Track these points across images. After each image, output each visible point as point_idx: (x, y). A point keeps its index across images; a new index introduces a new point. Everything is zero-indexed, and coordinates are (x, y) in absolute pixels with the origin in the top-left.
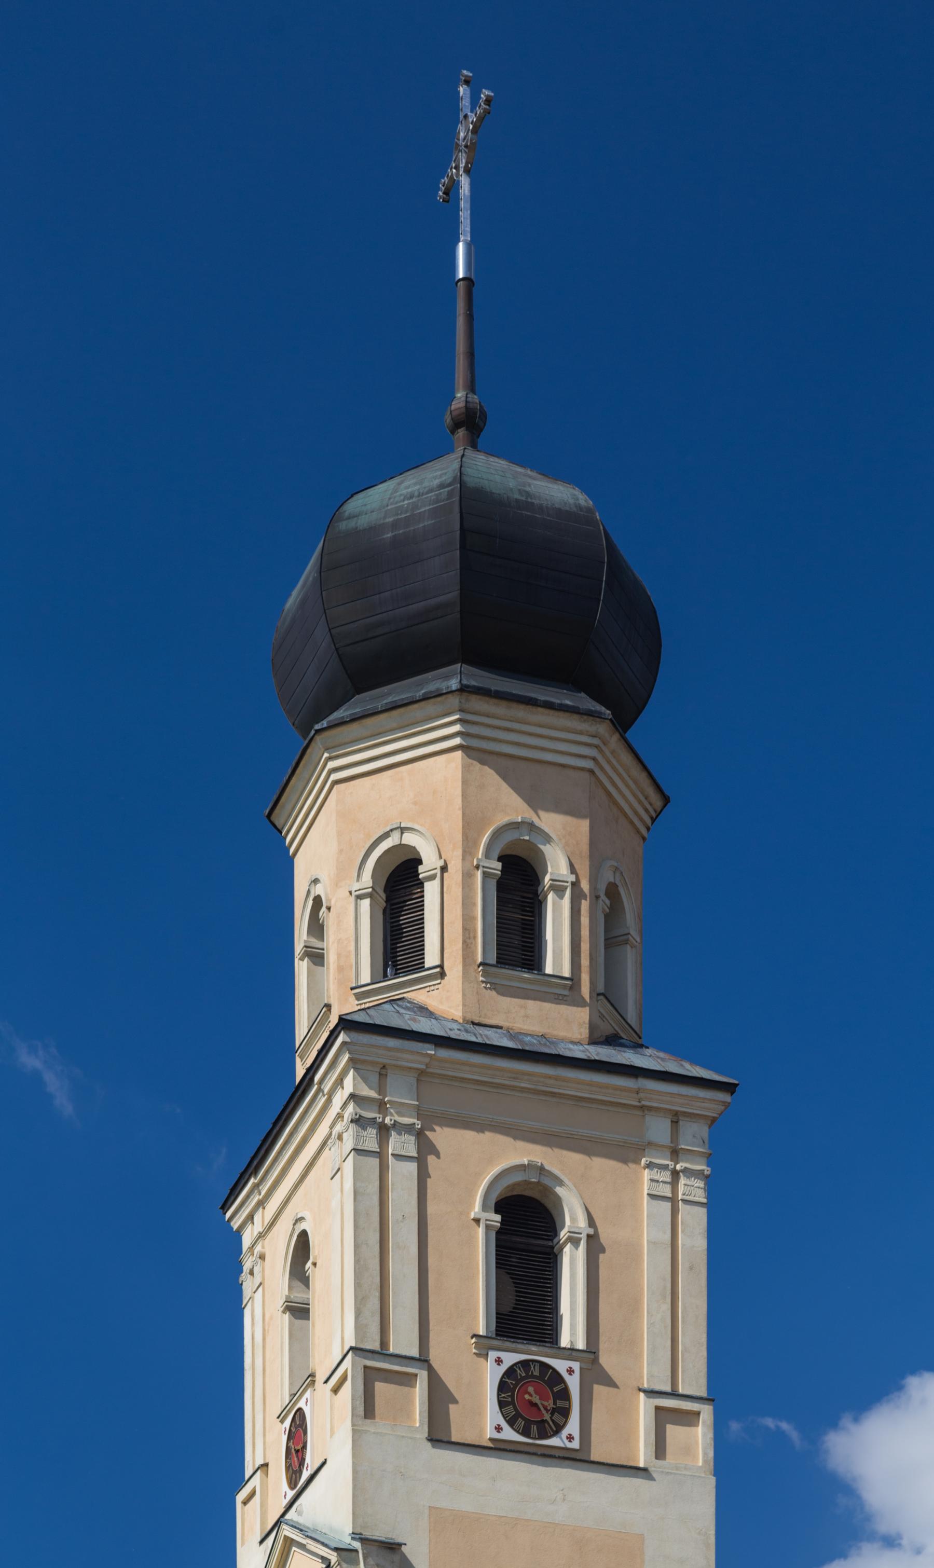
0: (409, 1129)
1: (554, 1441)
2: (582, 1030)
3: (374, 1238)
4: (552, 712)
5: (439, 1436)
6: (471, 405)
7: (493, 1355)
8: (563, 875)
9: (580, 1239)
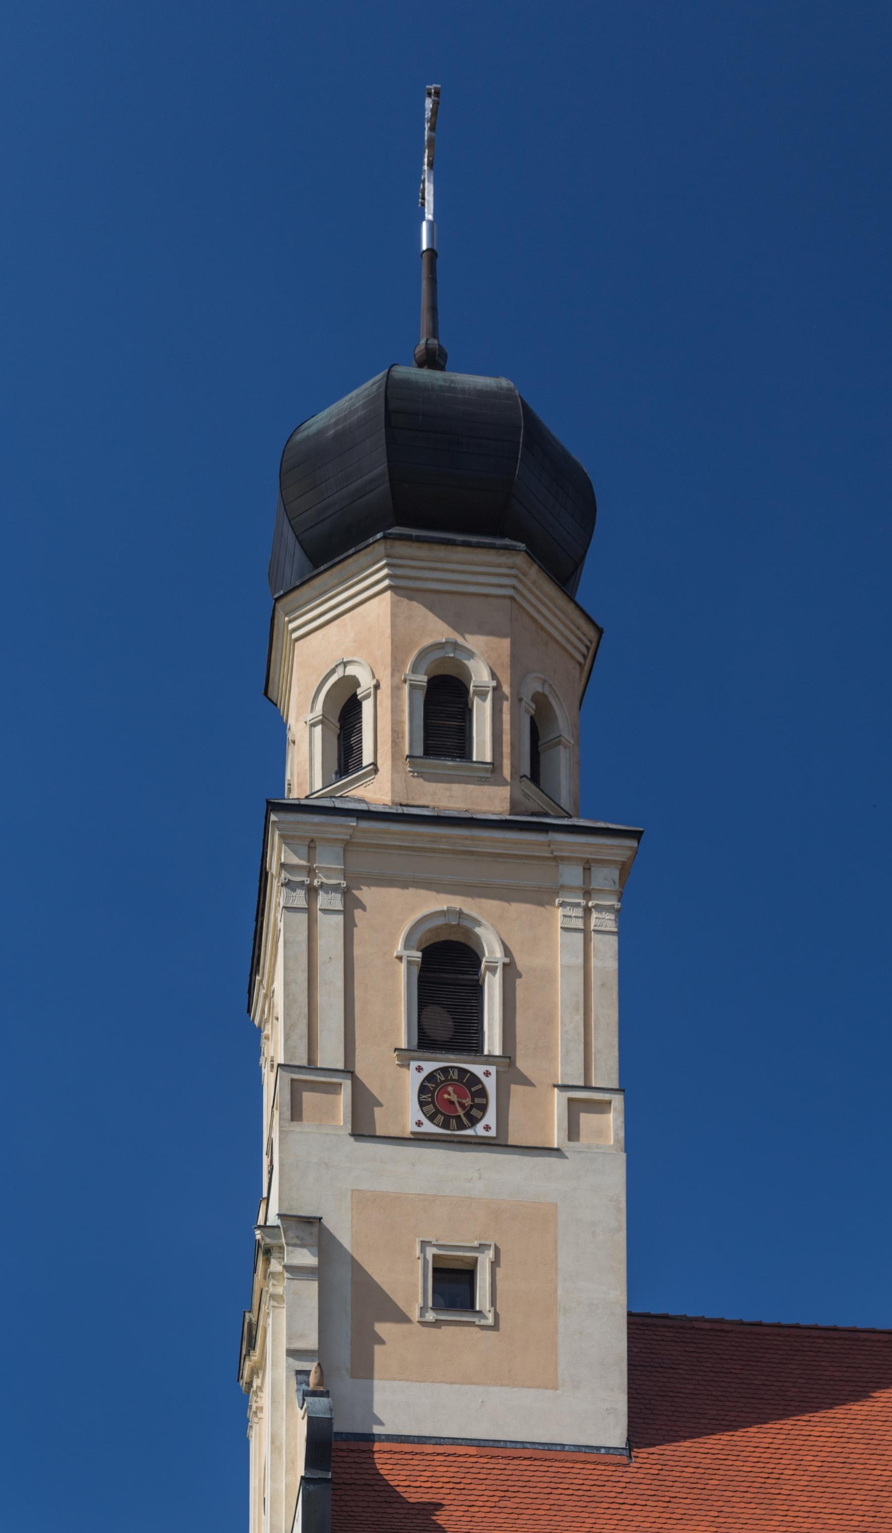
0: (335, 888)
1: (469, 1132)
2: (504, 804)
3: (303, 977)
4: (470, 550)
5: (362, 1129)
6: (431, 346)
7: (414, 1064)
8: (485, 682)
9: (497, 967)
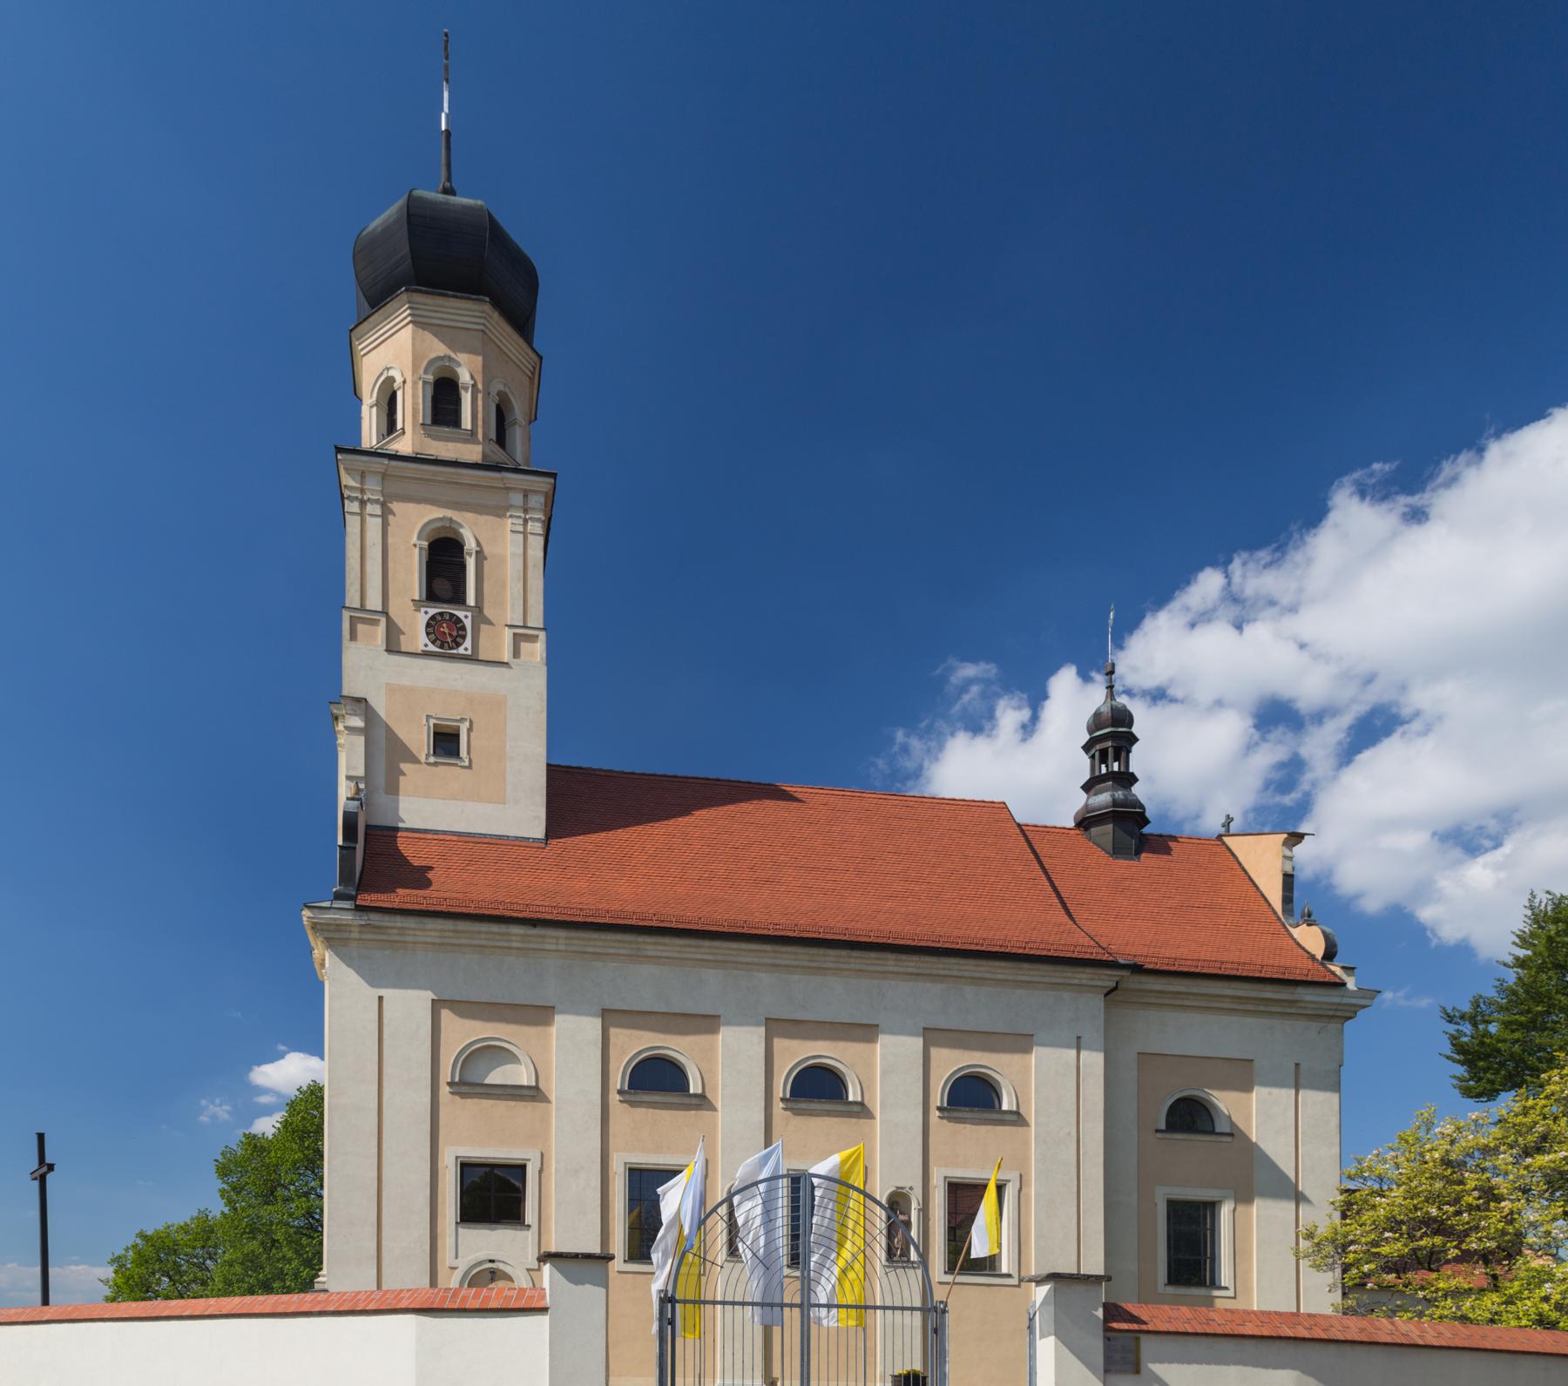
0: (377, 501)
5: (392, 648)
